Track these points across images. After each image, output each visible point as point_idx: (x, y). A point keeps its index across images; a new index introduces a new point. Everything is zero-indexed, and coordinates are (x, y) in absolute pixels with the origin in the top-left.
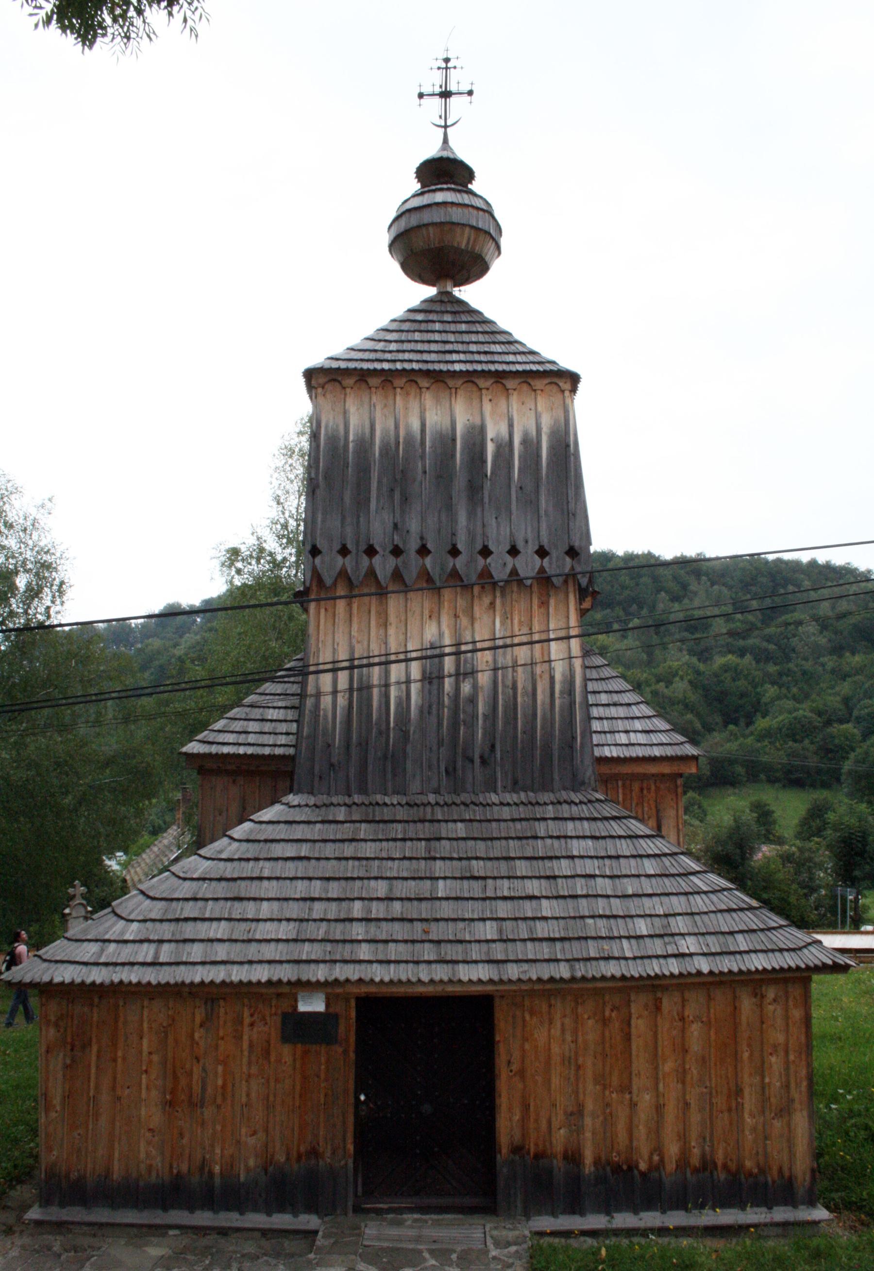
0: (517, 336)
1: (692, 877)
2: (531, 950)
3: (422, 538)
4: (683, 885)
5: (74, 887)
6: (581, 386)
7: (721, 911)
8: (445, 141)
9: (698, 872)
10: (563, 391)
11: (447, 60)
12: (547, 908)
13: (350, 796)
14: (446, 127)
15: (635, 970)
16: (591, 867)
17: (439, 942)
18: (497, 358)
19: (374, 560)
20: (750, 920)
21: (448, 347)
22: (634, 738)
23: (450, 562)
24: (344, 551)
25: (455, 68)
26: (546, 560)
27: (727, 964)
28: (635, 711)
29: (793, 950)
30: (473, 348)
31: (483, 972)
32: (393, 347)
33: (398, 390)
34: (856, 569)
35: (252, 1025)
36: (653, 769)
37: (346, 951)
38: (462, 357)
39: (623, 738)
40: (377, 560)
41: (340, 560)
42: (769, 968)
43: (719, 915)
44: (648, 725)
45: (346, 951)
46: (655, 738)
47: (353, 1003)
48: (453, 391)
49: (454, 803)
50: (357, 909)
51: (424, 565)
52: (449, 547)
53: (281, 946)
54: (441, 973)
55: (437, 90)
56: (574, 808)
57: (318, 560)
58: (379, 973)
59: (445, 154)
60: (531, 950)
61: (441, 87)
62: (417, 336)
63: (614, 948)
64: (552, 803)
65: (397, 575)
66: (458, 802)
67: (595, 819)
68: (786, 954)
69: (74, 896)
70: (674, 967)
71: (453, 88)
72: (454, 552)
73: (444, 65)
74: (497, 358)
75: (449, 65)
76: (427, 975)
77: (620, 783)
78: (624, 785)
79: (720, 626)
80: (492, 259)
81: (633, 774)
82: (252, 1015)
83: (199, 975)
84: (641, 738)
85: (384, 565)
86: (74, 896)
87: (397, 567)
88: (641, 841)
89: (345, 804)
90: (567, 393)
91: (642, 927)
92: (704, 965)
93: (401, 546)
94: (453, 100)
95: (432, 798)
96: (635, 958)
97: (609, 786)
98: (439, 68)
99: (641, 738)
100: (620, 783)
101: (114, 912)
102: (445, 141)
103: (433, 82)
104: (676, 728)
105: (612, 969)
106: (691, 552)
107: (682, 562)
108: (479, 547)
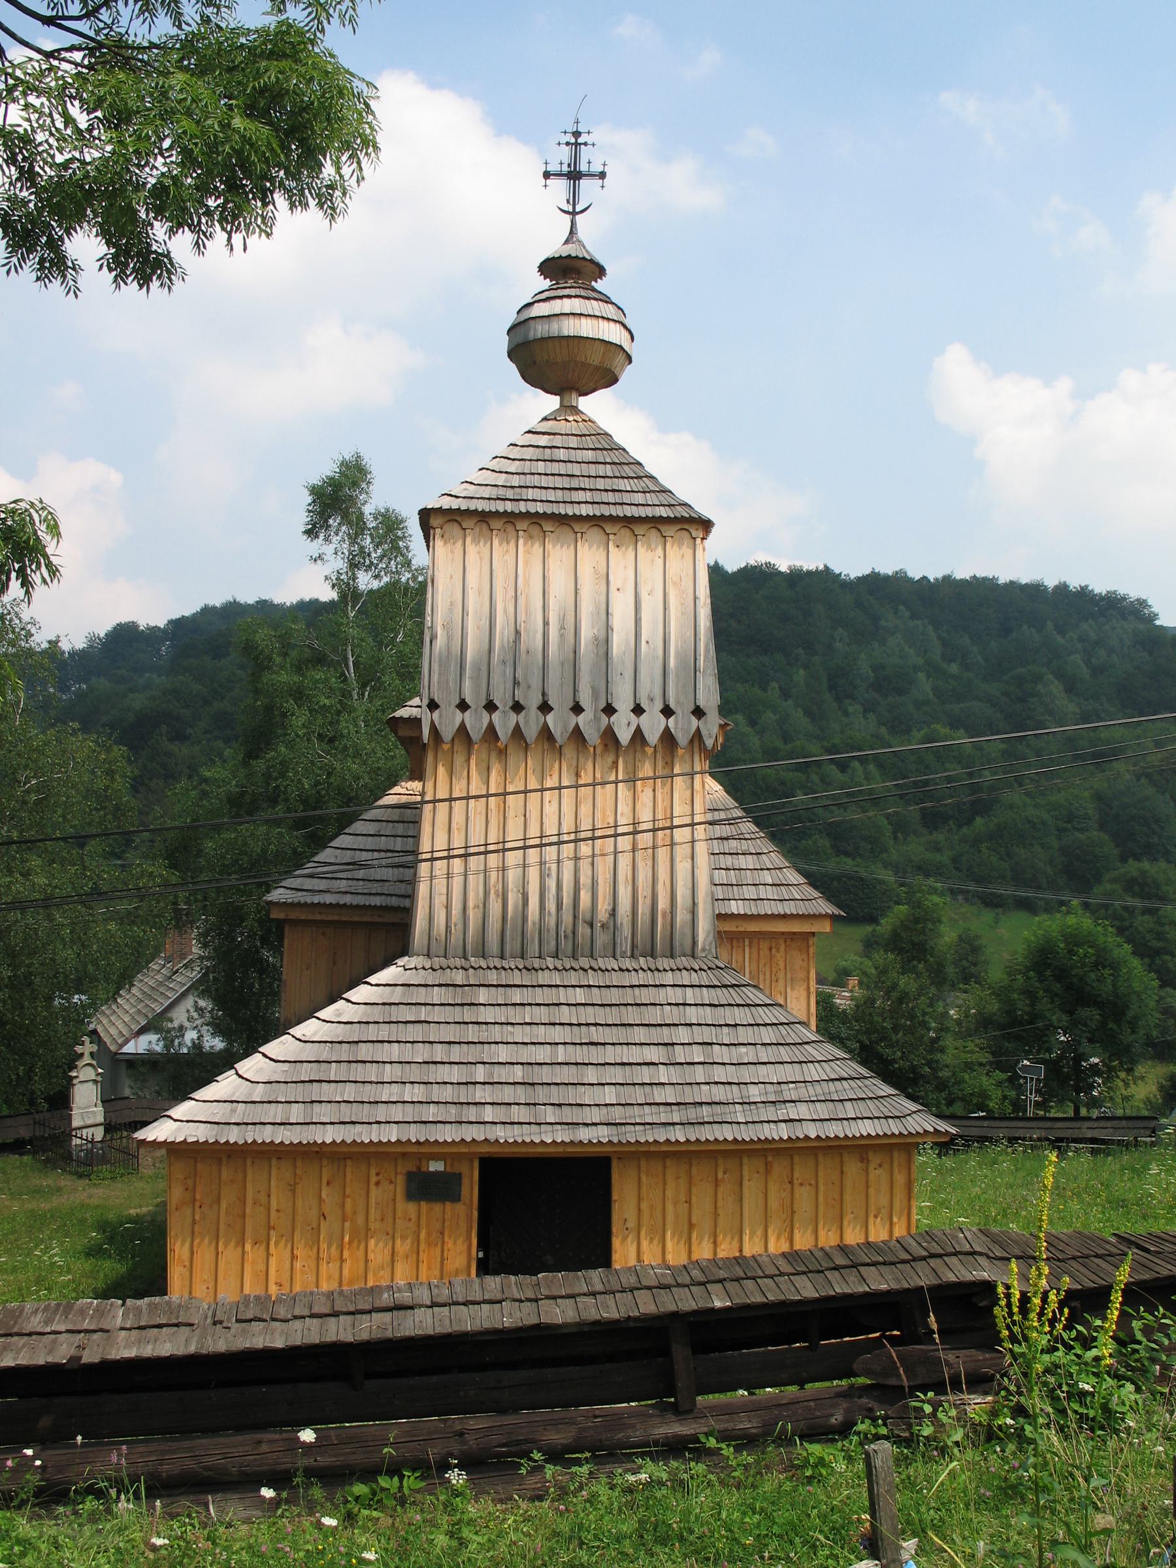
0: (650, 468)
1: (806, 1046)
2: (649, 1114)
3: (544, 694)
4: (797, 1054)
5: (83, 1044)
6: (714, 530)
7: (832, 1080)
8: (573, 231)
9: (813, 1042)
10: (695, 539)
11: (577, 134)
12: (663, 1075)
13: (466, 959)
14: (574, 213)
15: (747, 1133)
16: (706, 1035)
17: (560, 1105)
18: (627, 498)
19: (493, 716)
20: (847, 1089)
21: (575, 483)
22: (763, 892)
23: (573, 720)
24: (463, 706)
25: (585, 144)
26: (672, 720)
27: (834, 1130)
28: (766, 861)
29: (898, 1117)
30: (601, 484)
31: (603, 1134)
32: (516, 481)
33: (521, 533)
34: (1124, 599)
35: (377, 1183)
36: (782, 927)
37: (471, 1114)
38: (588, 496)
39: (750, 892)
40: (496, 717)
41: (459, 716)
42: (874, 1134)
43: (830, 1083)
44: (778, 877)
45: (471, 1114)
46: (784, 893)
47: (476, 1164)
48: (579, 535)
49: (572, 968)
50: (480, 1074)
51: (545, 723)
52: (571, 704)
53: (409, 1107)
54: (562, 1135)
55: (565, 169)
56: (745, 848)
57: (436, 714)
58: (501, 1134)
59: (571, 250)
60: (649, 1114)
61: (569, 165)
62: (541, 467)
63: (728, 1113)
64: (672, 970)
65: (517, 732)
66: (577, 967)
67: (714, 986)
68: (890, 1120)
69: (82, 1055)
70: (784, 1132)
71: (584, 168)
72: (577, 709)
73: (573, 140)
74: (627, 498)
75: (579, 141)
76: (549, 1134)
77: (747, 942)
78: (750, 943)
79: (924, 686)
80: (622, 369)
81: (760, 933)
82: (377, 1174)
83: (329, 1135)
84: (770, 893)
85: (504, 722)
86: (82, 1055)
87: (517, 726)
88: (759, 1009)
89: (462, 968)
90: (698, 541)
91: (754, 1093)
92: (812, 1131)
93: (522, 702)
94: (584, 183)
95: (550, 962)
96: (747, 1123)
97: (735, 944)
98: (568, 144)
99: (770, 893)
100: (747, 942)
101: (237, 1073)
102: (573, 231)
103: (560, 157)
104: (813, 880)
105: (728, 1133)
106: (887, 568)
107: (874, 583)
108: (603, 704)
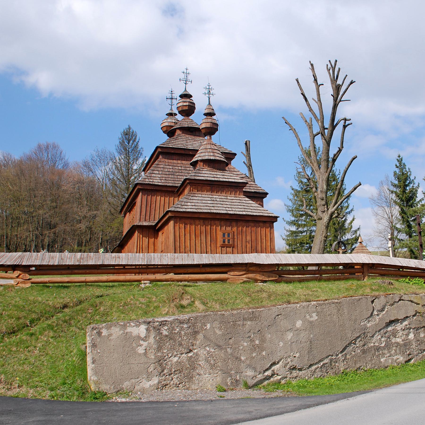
11: (172, 91)
